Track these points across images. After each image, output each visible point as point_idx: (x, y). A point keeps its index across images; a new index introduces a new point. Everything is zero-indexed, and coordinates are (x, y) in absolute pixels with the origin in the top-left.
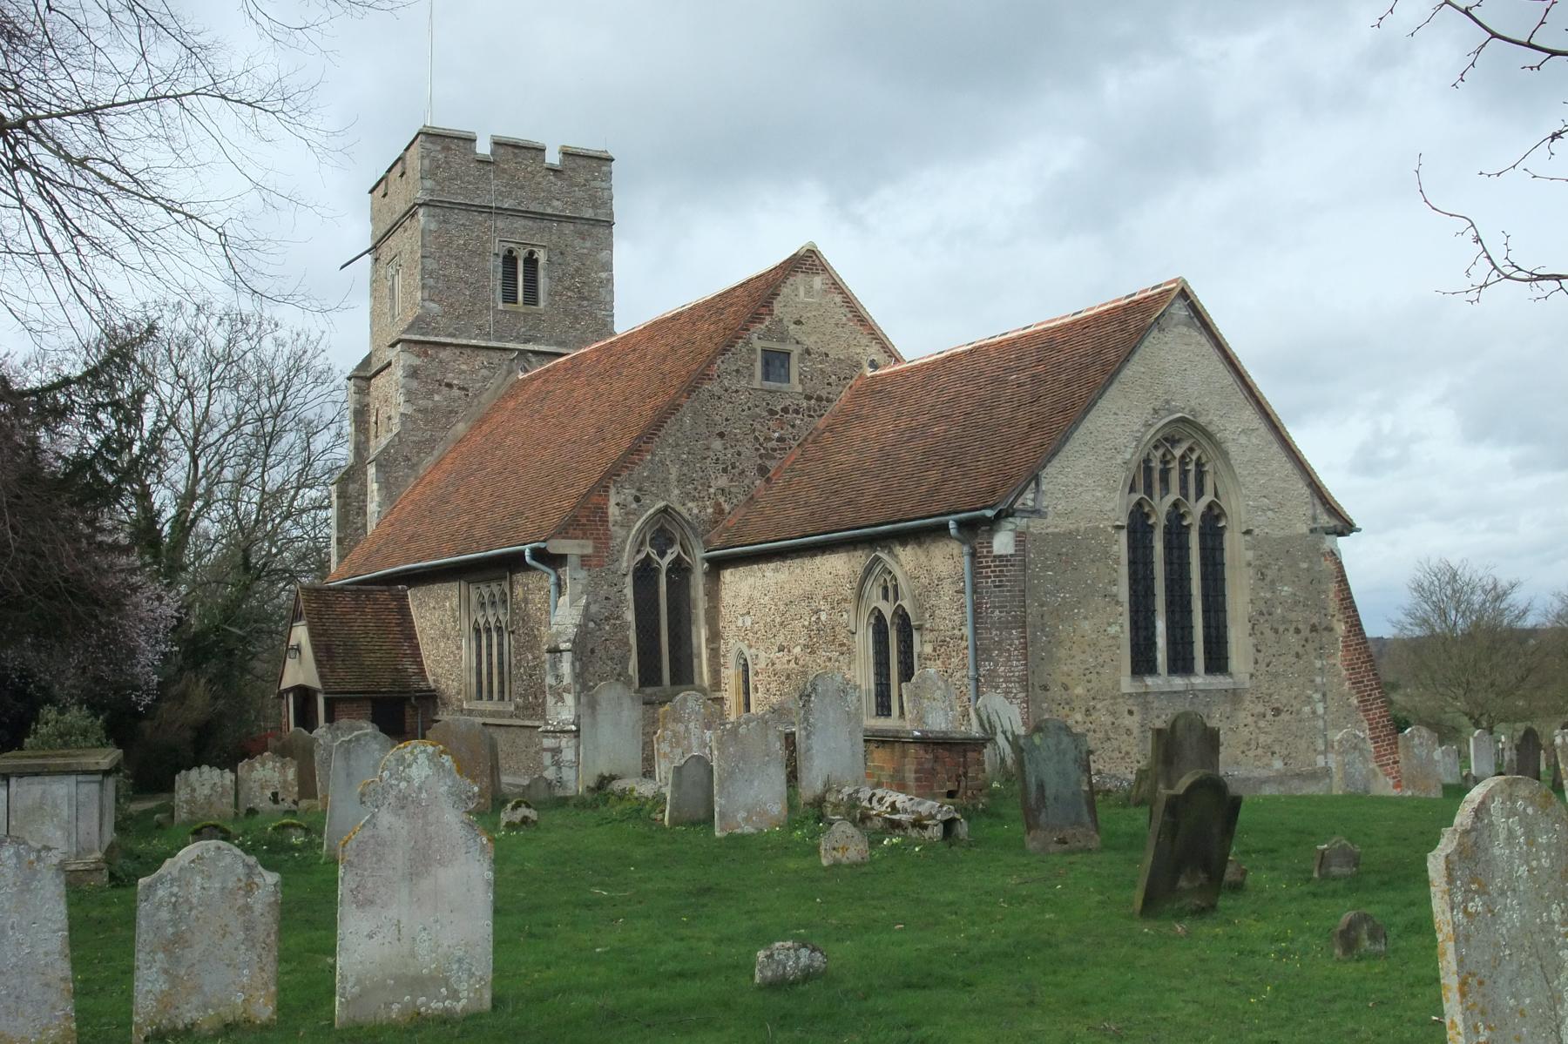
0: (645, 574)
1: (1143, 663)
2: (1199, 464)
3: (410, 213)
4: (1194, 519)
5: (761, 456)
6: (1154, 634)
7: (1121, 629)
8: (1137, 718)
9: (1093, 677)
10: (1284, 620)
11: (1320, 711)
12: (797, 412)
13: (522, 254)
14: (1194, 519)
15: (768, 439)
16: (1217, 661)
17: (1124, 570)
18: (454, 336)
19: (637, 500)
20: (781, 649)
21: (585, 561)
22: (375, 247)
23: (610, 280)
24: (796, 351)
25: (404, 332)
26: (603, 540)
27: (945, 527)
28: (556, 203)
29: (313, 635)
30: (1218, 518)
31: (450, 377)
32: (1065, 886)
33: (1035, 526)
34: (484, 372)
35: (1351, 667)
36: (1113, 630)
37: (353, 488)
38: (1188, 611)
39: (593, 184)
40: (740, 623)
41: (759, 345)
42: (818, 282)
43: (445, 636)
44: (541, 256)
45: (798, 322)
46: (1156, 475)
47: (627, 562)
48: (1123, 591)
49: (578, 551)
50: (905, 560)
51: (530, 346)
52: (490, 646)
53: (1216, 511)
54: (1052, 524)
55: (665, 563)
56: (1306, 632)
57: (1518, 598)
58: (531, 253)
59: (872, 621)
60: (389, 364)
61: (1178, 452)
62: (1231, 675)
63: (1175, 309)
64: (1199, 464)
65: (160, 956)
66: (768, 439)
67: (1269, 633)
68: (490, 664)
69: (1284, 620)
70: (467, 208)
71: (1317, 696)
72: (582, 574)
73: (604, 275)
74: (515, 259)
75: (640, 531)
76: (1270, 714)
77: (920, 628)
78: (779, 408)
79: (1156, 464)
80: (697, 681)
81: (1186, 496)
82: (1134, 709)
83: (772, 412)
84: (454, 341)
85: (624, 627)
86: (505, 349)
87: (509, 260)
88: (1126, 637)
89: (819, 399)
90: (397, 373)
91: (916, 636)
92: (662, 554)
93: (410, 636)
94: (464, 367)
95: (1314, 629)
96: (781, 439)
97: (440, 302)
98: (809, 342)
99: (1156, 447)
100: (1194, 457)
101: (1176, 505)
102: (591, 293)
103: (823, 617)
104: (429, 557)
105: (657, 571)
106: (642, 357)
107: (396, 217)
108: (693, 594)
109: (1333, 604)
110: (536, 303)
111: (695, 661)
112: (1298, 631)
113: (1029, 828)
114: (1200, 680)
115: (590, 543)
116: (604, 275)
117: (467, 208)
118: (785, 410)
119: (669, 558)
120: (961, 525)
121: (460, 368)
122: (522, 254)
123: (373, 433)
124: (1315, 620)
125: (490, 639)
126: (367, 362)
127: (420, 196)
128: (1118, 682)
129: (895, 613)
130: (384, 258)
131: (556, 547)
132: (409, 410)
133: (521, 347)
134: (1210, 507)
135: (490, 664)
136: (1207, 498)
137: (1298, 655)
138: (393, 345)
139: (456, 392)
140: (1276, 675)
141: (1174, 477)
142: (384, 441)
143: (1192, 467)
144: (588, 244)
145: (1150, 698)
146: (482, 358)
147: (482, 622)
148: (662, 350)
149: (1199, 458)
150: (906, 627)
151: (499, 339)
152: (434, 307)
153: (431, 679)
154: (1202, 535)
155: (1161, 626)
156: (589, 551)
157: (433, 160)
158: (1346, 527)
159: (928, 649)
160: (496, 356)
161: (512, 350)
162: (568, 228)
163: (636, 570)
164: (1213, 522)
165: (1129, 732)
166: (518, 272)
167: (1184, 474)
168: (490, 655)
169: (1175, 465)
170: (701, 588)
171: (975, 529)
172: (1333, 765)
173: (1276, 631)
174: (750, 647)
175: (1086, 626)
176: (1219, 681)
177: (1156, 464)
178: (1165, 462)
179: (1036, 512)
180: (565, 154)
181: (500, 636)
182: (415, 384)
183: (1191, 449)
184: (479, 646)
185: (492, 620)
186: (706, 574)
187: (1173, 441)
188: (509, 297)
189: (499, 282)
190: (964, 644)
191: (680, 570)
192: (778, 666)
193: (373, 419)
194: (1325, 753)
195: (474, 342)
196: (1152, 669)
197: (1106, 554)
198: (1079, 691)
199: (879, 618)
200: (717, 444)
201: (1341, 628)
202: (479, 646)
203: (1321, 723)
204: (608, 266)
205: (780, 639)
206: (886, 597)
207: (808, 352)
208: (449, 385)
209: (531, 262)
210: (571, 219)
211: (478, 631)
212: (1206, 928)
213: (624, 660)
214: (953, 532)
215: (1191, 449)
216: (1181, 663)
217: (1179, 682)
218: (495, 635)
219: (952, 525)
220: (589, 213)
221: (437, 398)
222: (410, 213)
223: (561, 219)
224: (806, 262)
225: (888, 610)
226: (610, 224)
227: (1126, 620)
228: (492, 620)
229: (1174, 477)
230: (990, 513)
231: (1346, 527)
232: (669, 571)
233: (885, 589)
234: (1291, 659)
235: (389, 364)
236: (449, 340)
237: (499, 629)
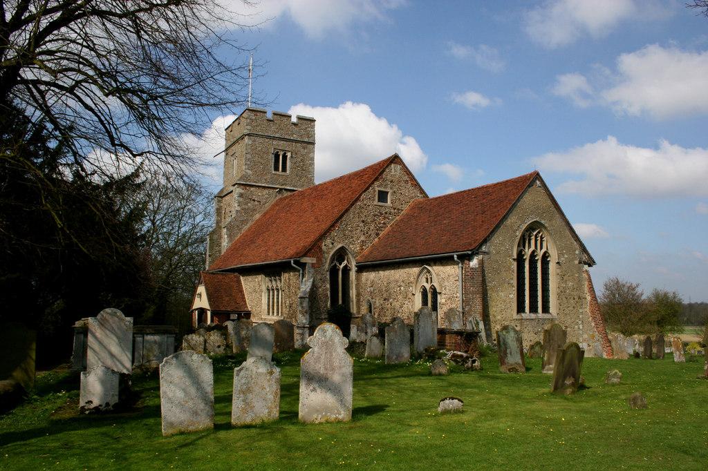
0: (334, 271)
1: (521, 309)
3: (242, 138)
4: (539, 257)
5: (377, 230)
7: (513, 296)
10: (570, 295)
11: (581, 327)
12: (390, 214)
13: (281, 154)
14: (539, 257)
15: (380, 223)
17: (515, 275)
18: (256, 182)
19: (333, 244)
22: (226, 150)
23: (313, 164)
25: (239, 180)
26: (319, 260)
27: (453, 257)
29: (207, 290)
30: (547, 257)
32: (59, 464)
35: (592, 312)
37: (215, 237)
38: (536, 291)
41: (377, 189)
43: (255, 291)
44: (289, 155)
47: (327, 266)
48: (515, 282)
50: (436, 270)
52: (273, 295)
53: (547, 255)
56: (577, 299)
57: (639, 291)
59: (422, 290)
60: (232, 192)
61: (535, 233)
64: (542, 238)
66: (380, 223)
68: (273, 302)
69: (570, 295)
70: (262, 136)
71: (580, 322)
72: (312, 270)
74: (279, 155)
75: (333, 255)
77: (440, 293)
84: (257, 184)
89: (399, 209)
90: (235, 195)
91: (439, 296)
92: (340, 264)
93: (241, 291)
94: (260, 194)
95: (579, 298)
96: (384, 223)
99: (527, 231)
100: (540, 235)
101: (533, 252)
102: (306, 166)
103: (402, 288)
104: (249, 263)
105: (339, 270)
106: (331, 192)
109: (586, 289)
111: (351, 303)
113: (502, 364)
115: (315, 259)
117: (262, 136)
118: (386, 213)
120: (459, 257)
121: (258, 194)
123: (223, 217)
125: (273, 292)
126: (222, 191)
127: (246, 132)
129: (431, 288)
130: (230, 154)
132: (238, 208)
133: (280, 187)
134: (545, 253)
135: (273, 302)
137: (574, 307)
138: (234, 185)
140: (566, 314)
142: (228, 220)
143: (539, 238)
144: (306, 151)
145: (523, 321)
147: (270, 286)
148: (339, 190)
149: (542, 236)
150: (435, 293)
151: (273, 184)
152: (250, 172)
153: (249, 307)
156: (314, 262)
158: (591, 263)
159: (443, 301)
160: (271, 191)
161: (277, 188)
162: (299, 145)
166: (279, 161)
167: (536, 241)
168: (273, 299)
174: (372, 298)
180: (274, 114)
181: (278, 292)
183: (539, 232)
184: (269, 295)
185: (275, 286)
188: (276, 169)
190: (457, 299)
191: (346, 270)
195: (263, 185)
196: (524, 311)
197: (509, 268)
198: (499, 317)
200: (361, 224)
201: (589, 298)
202: (269, 295)
204: (313, 159)
205: (385, 296)
206: (427, 282)
208: (254, 200)
211: (268, 290)
214: (456, 259)
215: (539, 232)
217: (533, 316)
218: (271, 292)
219: (455, 256)
220: (306, 140)
222: (242, 138)
223: (296, 141)
224: (395, 159)
225: (428, 286)
226: (313, 144)
227: (515, 292)
228: (275, 286)
230: (470, 252)
231: (591, 263)
233: (427, 279)
234: (571, 308)
235: (232, 192)
236: (254, 184)
237: (278, 290)
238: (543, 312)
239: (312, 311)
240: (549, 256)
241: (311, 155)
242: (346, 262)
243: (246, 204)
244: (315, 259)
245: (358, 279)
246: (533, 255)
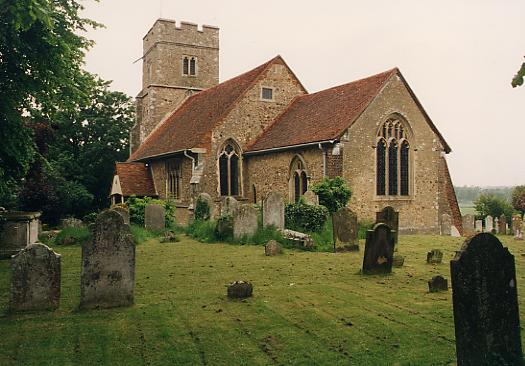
0: (223, 159)
1: (381, 192)
7: (374, 180)
14: (399, 145)
16: (405, 192)
44: (196, 59)
50: (305, 159)
55: (230, 156)
61: (394, 124)
63: (391, 82)
64: (401, 127)
82: (348, 330)
83: (265, 109)
87: (186, 60)
114: (399, 197)
116: (216, 59)
119: (232, 153)
122: (190, 58)
126: (142, 92)
131: (193, 150)
136: (403, 139)
146: (177, 91)
158: (447, 150)
164: (405, 144)
171: (328, 147)
176: (405, 198)
177: (387, 128)
187: (393, 120)
191: (234, 159)
193: (387, 323)
209: (193, 61)
216: (393, 192)
217: (392, 198)
220: (211, 46)
225: (299, 172)
229: (393, 132)
243: (159, 103)
246: (393, 143)
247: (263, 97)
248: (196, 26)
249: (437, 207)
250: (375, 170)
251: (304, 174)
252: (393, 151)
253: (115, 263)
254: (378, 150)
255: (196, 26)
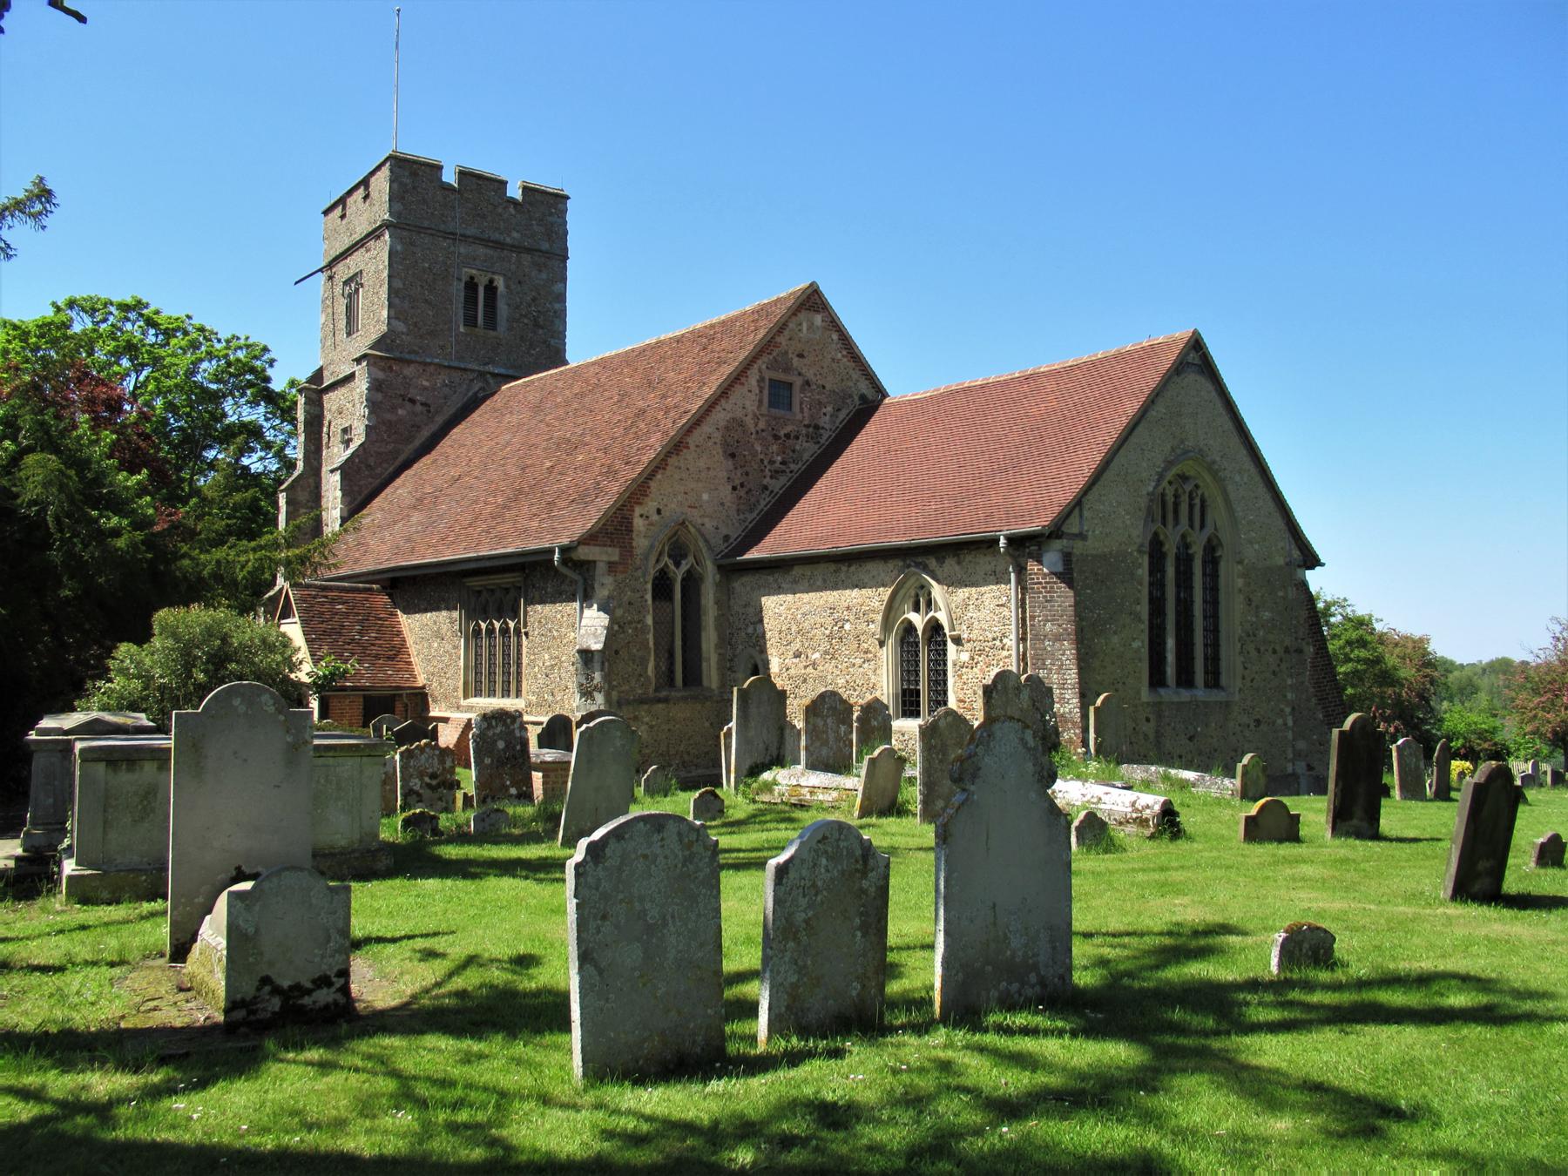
1: (1157, 680)
2: (1203, 502)
4: (1197, 550)
6: (1164, 650)
7: (1141, 644)
8: (1153, 724)
9: (1120, 686)
13: (482, 281)
14: (1197, 550)
16: (1213, 680)
20: (797, 655)
21: (612, 567)
24: (798, 382)
26: (627, 550)
28: (515, 235)
31: (413, 393)
33: (1078, 547)
34: (446, 390)
36: (1136, 645)
39: (550, 219)
40: (750, 630)
42: (818, 319)
44: (500, 283)
45: (801, 356)
46: (1170, 507)
48: (1144, 609)
49: (605, 558)
51: (491, 368)
54: (1093, 546)
58: (491, 281)
62: (1222, 688)
65: (791, 944)
67: (1254, 653)
71: (1288, 710)
73: (557, 306)
74: (476, 285)
76: (1252, 725)
78: (782, 433)
79: (1170, 499)
80: (705, 683)
81: (1191, 526)
83: (776, 437)
85: (644, 630)
86: (465, 370)
87: (471, 286)
88: (1145, 652)
92: (677, 564)
94: (426, 383)
95: (1287, 650)
97: (405, 321)
98: (810, 375)
107: (357, 237)
108: (703, 602)
110: (494, 329)
111: (704, 664)
112: (1275, 652)
114: (1200, 693)
116: (557, 306)
118: (787, 436)
119: (684, 567)
124: (1287, 642)
128: (1138, 692)
136: (1209, 530)
137: (1274, 673)
139: (419, 408)
141: (1184, 508)
144: (544, 276)
154: (1204, 562)
155: (1171, 643)
156: (616, 558)
157: (401, 183)
158: (1312, 561)
160: (456, 375)
161: (472, 371)
162: (526, 259)
163: (655, 579)
164: (1211, 548)
165: (1146, 736)
167: (1191, 507)
169: (1185, 499)
170: (711, 597)
172: (1299, 771)
173: (1258, 651)
175: (1115, 639)
176: (1216, 696)
177: (1170, 499)
178: (1176, 496)
179: (1081, 536)
182: (379, 396)
186: (718, 585)
188: (471, 321)
189: (461, 305)
190: (1005, 653)
192: (792, 672)
194: (1293, 761)
199: (910, 628)
203: (1290, 735)
205: (796, 646)
207: (808, 383)
208: (412, 401)
210: (529, 250)
212: (1179, 918)
213: (643, 662)
217: (1185, 695)
221: (400, 412)
223: (515, 248)
225: (918, 620)
229: (1184, 508)
232: (683, 580)
238: (1207, 685)
239: (611, 688)
240: (1220, 544)
241: (557, 287)
242: (691, 559)
243: (394, 408)
244: (617, 550)
245: (723, 604)
246: (1185, 545)
247: (165, 898)
248: (504, 183)
249: (1290, 723)
250: (1145, 616)
251: (935, 628)
252: (1184, 561)
253: (32, 1050)
254: (1151, 557)
255: (504, 183)
